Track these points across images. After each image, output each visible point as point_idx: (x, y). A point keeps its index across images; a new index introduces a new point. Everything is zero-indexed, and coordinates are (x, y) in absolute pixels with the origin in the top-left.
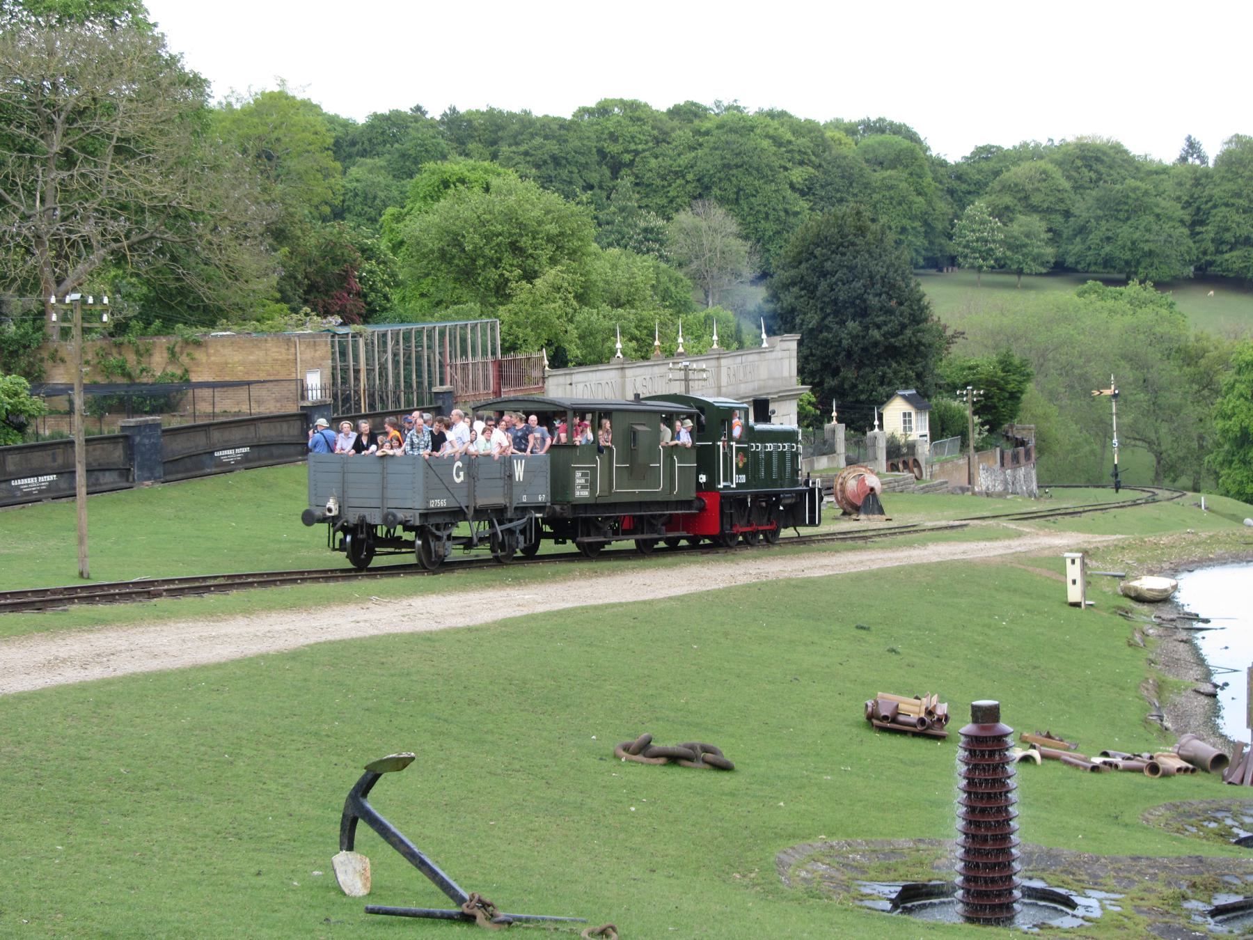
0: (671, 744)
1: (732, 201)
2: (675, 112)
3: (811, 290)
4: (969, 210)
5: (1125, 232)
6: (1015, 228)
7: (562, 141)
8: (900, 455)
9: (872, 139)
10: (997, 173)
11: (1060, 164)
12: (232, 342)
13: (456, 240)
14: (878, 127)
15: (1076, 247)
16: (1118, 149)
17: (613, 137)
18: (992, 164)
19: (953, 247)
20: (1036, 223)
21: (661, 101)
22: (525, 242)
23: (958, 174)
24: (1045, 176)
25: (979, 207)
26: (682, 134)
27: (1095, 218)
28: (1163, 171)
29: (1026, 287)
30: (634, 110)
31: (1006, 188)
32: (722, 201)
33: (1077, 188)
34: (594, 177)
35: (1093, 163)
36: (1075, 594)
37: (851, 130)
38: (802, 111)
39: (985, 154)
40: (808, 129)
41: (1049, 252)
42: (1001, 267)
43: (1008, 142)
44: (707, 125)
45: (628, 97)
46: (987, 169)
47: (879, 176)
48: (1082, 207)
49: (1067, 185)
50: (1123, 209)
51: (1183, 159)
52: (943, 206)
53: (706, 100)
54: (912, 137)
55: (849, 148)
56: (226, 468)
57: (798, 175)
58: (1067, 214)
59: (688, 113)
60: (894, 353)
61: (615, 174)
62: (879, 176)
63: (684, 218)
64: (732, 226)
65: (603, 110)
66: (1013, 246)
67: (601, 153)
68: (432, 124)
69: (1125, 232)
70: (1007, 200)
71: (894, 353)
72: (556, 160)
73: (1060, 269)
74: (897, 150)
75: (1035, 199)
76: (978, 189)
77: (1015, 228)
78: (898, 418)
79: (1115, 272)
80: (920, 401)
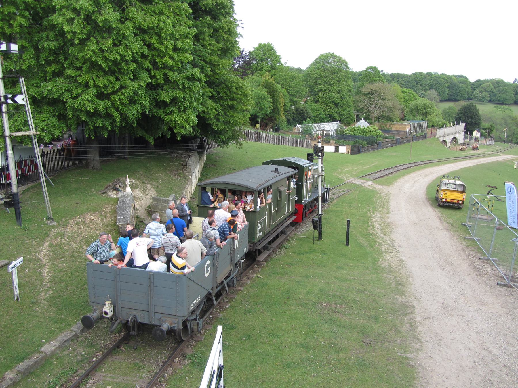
0: (492, 186)
1: (436, 89)
2: (427, 74)
3: (464, 114)
4: (475, 91)
5: (503, 95)
6: (483, 94)
7: (409, 79)
8: (476, 139)
9: (460, 79)
10: (481, 84)
11: (492, 83)
12: (398, 124)
13: (416, 107)
14: (460, 76)
15: (494, 98)
16: (503, 81)
17: (417, 78)
18: (479, 83)
19: (471, 97)
20: (487, 94)
21: (425, 72)
22: (426, 108)
23: (473, 84)
24: (489, 85)
25: (477, 91)
26: (429, 78)
27: (499, 93)
28: (511, 85)
29: (484, 104)
30: (421, 74)
31: (482, 87)
32: (435, 89)
33: (495, 88)
34: (414, 84)
35: (498, 83)
36: (515, 167)
37: (456, 76)
38: (447, 74)
39: (478, 81)
40: (448, 77)
41: (489, 99)
42: (480, 101)
43: (482, 78)
44: (433, 76)
45: (420, 71)
46: (479, 84)
47: (461, 85)
48: (495, 91)
49: (493, 87)
50: (504, 92)
51: (514, 82)
52: (471, 90)
53: (432, 72)
54: (466, 78)
55: (455, 80)
56: (405, 143)
57: (447, 85)
58: (492, 92)
59: (429, 74)
60: (475, 124)
61: (417, 84)
62: (461, 85)
63: (429, 92)
64: (437, 94)
65: (416, 74)
66: (483, 97)
67: (415, 81)
68: (388, 75)
69: (503, 95)
70: (482, 89)
71: (475, 124)
72: (408, 82)
73: (490, 101)
74: (463, 80)
75: (487, 90)
76: (477, 87)
77: (483, 94)
78: (476, 134)
79: (501, 102)
80: (478, 131)
